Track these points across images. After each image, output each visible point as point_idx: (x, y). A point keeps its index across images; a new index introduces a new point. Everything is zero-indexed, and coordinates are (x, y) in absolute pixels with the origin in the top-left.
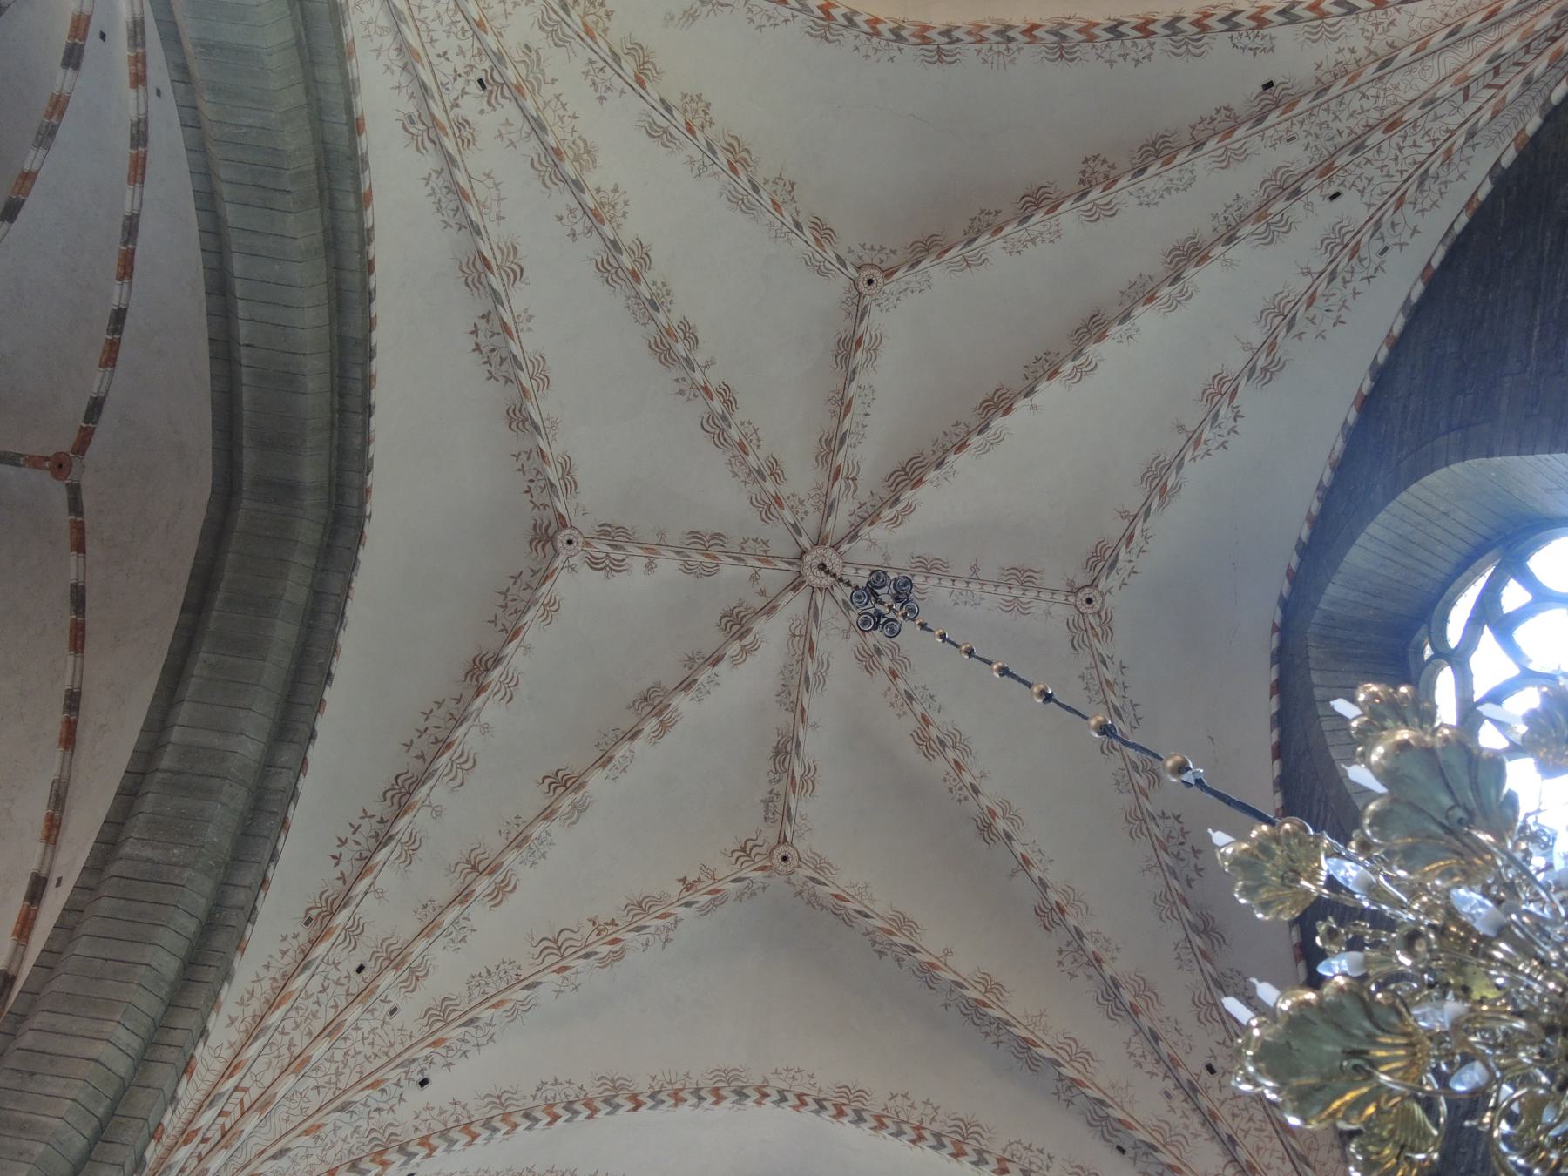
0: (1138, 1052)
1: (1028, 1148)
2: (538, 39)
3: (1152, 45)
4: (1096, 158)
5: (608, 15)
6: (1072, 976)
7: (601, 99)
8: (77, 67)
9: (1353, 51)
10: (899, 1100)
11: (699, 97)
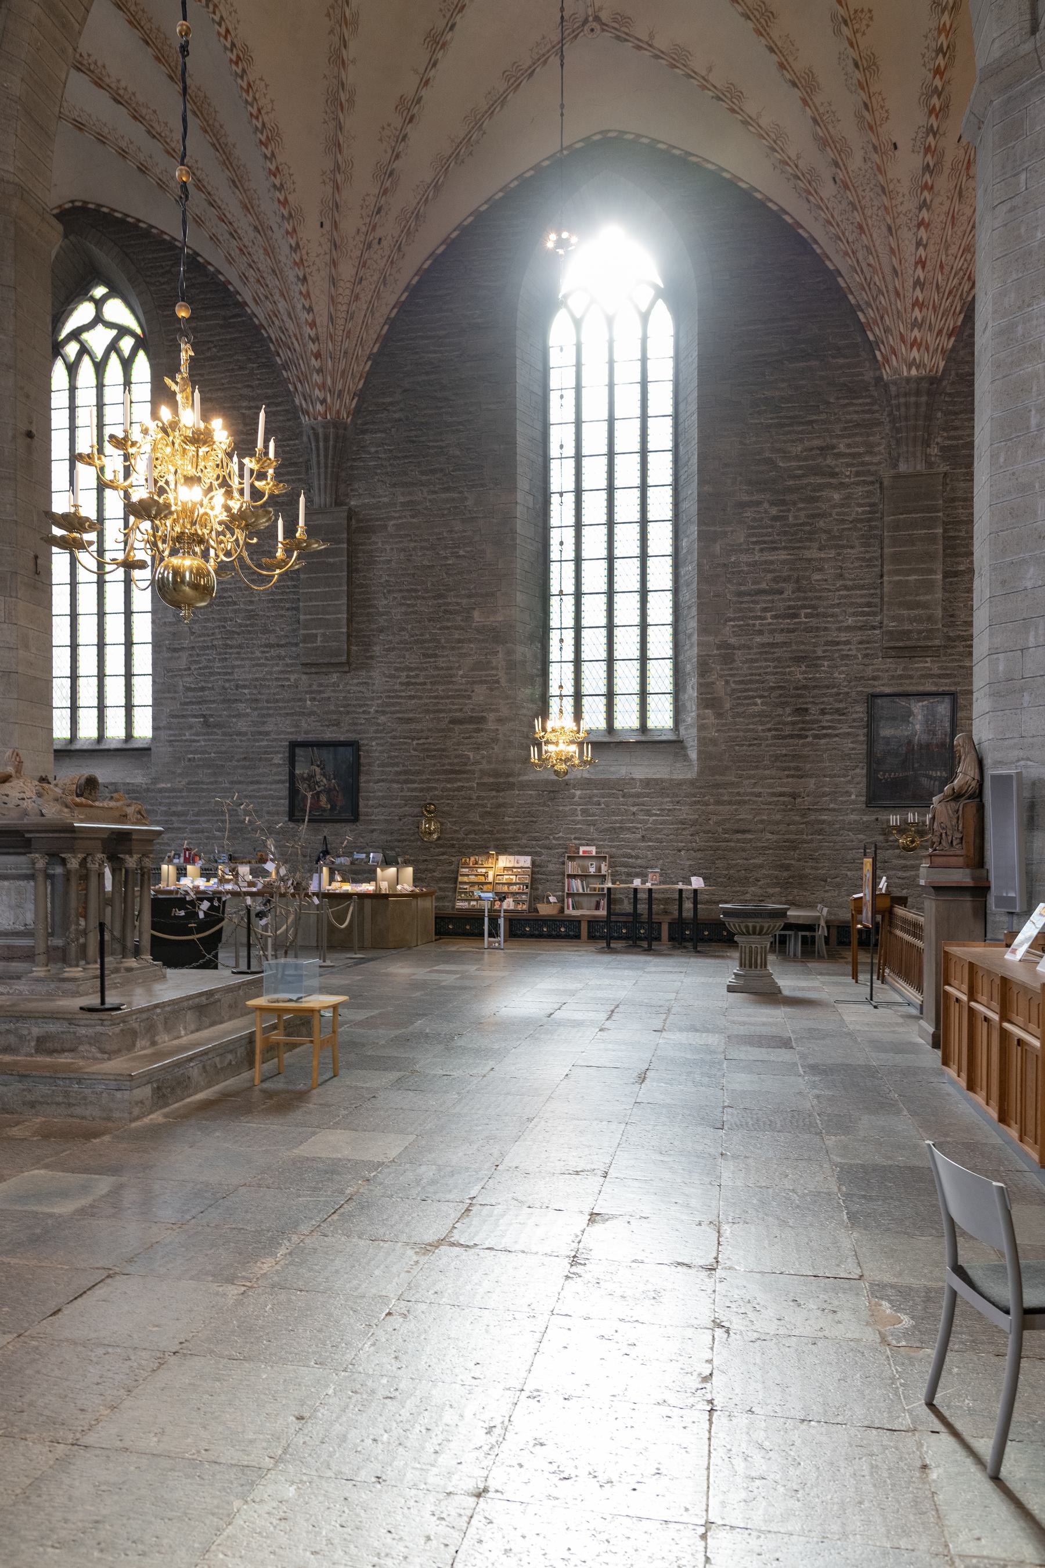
0: (367, 203)
1: (291, 175)
3: (930, 70)
4: (871, 18)
6: (381, 140)
9: (902, 203)
10: (263, 84)
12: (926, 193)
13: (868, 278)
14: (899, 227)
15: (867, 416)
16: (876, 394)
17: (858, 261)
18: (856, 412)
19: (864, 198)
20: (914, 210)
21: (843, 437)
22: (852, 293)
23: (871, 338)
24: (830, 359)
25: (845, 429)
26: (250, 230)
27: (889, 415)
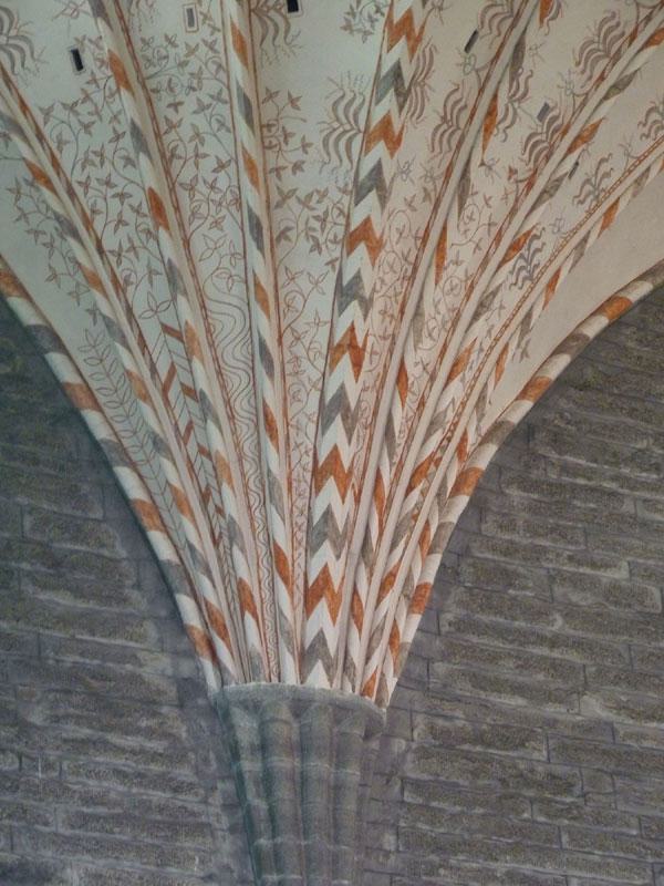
9: (297, 167)
12: (380, 150)
13: (163, 372)
14: (283, 234)
15: (158, 796)
16: (182, 731)
17: (129, 311)
18: (120, 774)
19: (172, 126)
20: (335, 195)
21: (73, 844)
22: (98, 407)
23: (165, 551)
24: (29, 589)
25: (84, 820)
26: (474, 204)
27: (229, 807)
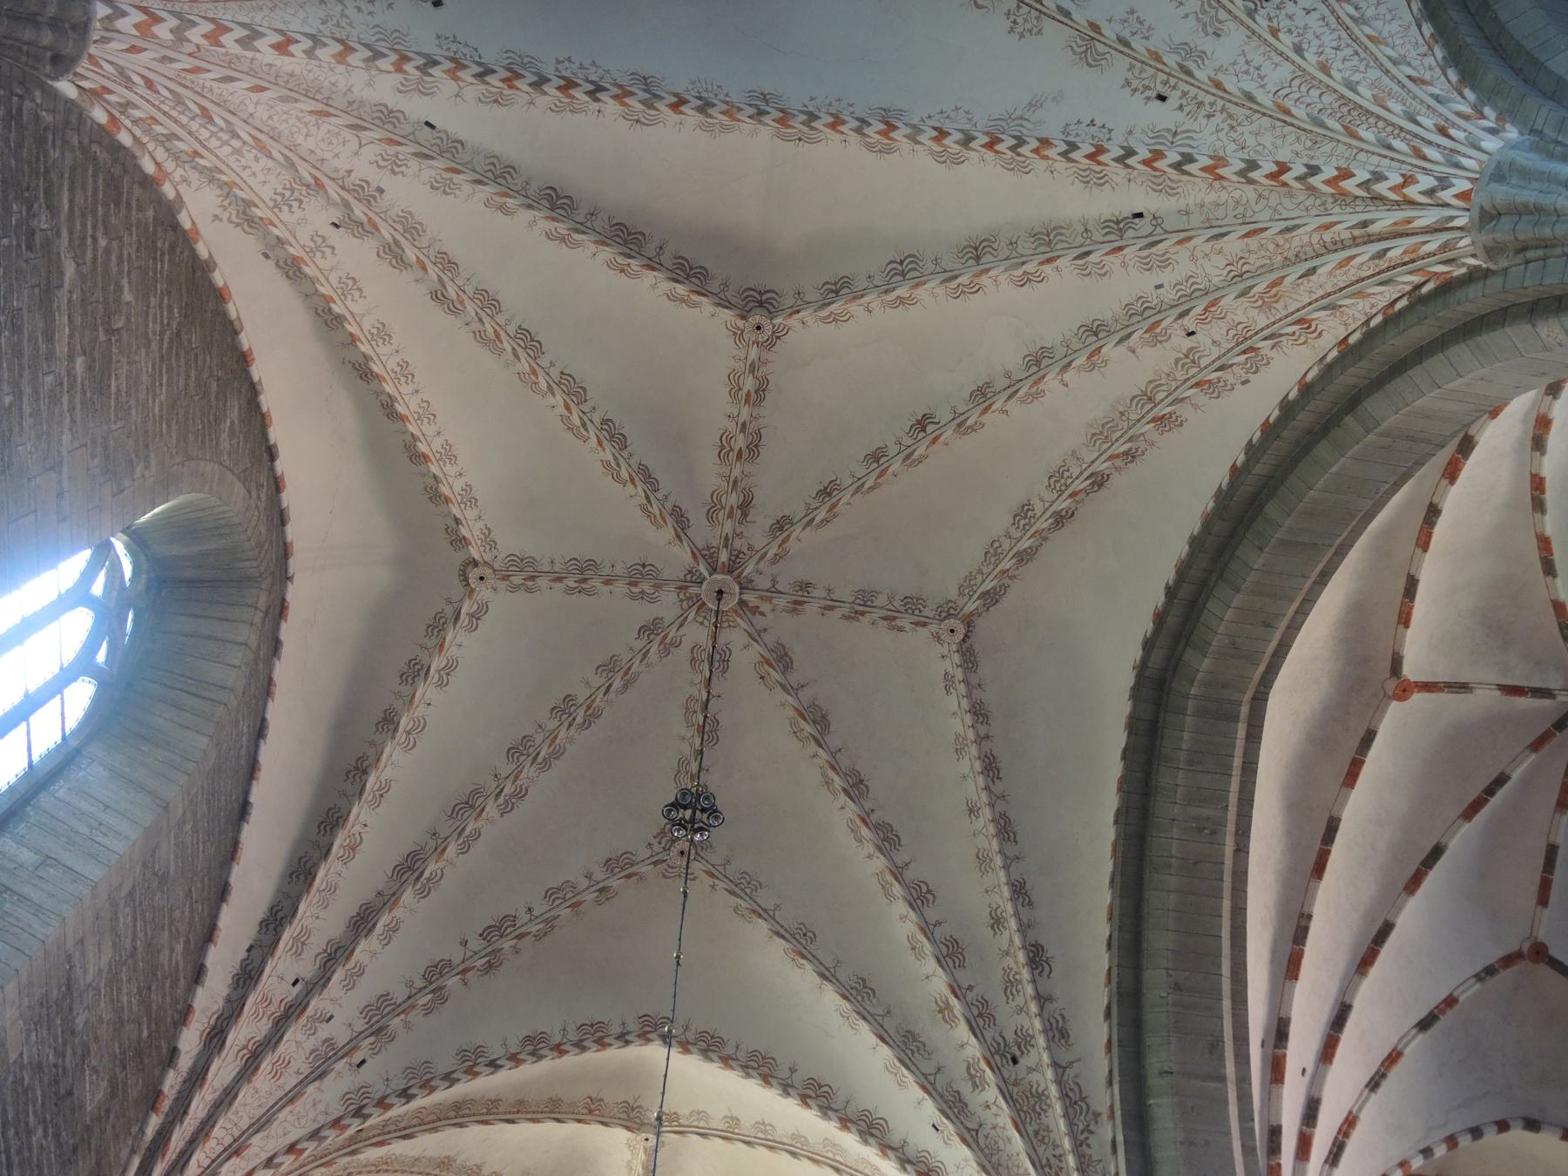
2: (1207, 44)
5: (1128, 83)
7: (1132, 12)
8: (1502, 773)
11: (1022, 36)
